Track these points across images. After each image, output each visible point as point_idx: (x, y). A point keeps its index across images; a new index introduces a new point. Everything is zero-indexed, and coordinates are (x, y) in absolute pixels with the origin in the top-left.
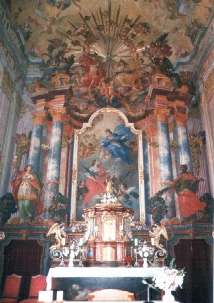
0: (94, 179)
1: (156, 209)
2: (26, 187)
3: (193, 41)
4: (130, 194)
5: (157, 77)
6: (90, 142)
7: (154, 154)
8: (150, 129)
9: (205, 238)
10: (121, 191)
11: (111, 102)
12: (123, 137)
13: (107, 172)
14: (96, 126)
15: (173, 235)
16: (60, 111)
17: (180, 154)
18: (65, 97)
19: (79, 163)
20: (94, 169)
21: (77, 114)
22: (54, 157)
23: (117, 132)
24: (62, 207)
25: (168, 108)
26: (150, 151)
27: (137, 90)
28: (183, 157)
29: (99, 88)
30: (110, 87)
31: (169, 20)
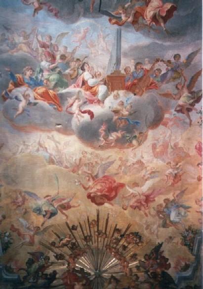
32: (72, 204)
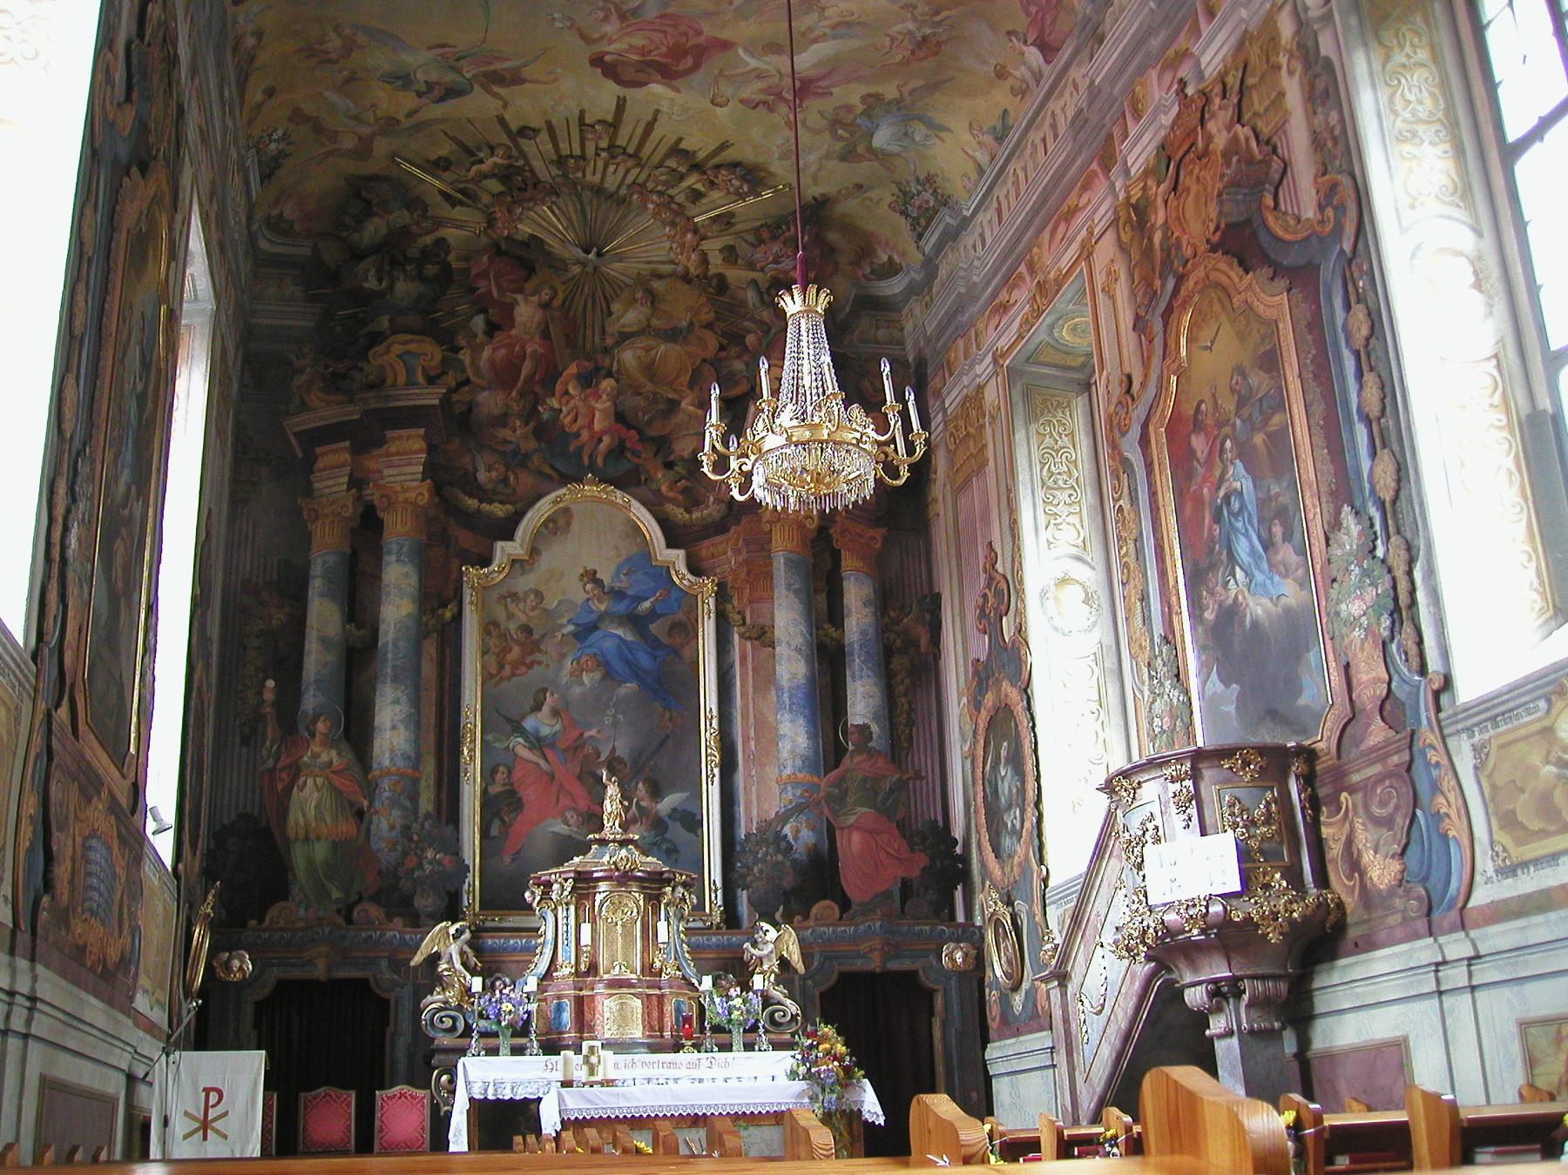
0: (542, 762)
1: (761, 871)
3: (920, 236)
4: (670, 816)
6: (523, 619)
8: (743, 575)
9: (918, 965)
11: (600, 461)
12: (647, 604)
14: (544, 554)
15: (817, 957)
16: (412, 495)
18: (426, 438)
20: (542, 723)
21: (472, 503)
23: (623, 583)
24: (440, 863)
28: (860, 689)
29: (556, 406)
30: (598, 405)
31: (832, 164)
32: (525, 73)
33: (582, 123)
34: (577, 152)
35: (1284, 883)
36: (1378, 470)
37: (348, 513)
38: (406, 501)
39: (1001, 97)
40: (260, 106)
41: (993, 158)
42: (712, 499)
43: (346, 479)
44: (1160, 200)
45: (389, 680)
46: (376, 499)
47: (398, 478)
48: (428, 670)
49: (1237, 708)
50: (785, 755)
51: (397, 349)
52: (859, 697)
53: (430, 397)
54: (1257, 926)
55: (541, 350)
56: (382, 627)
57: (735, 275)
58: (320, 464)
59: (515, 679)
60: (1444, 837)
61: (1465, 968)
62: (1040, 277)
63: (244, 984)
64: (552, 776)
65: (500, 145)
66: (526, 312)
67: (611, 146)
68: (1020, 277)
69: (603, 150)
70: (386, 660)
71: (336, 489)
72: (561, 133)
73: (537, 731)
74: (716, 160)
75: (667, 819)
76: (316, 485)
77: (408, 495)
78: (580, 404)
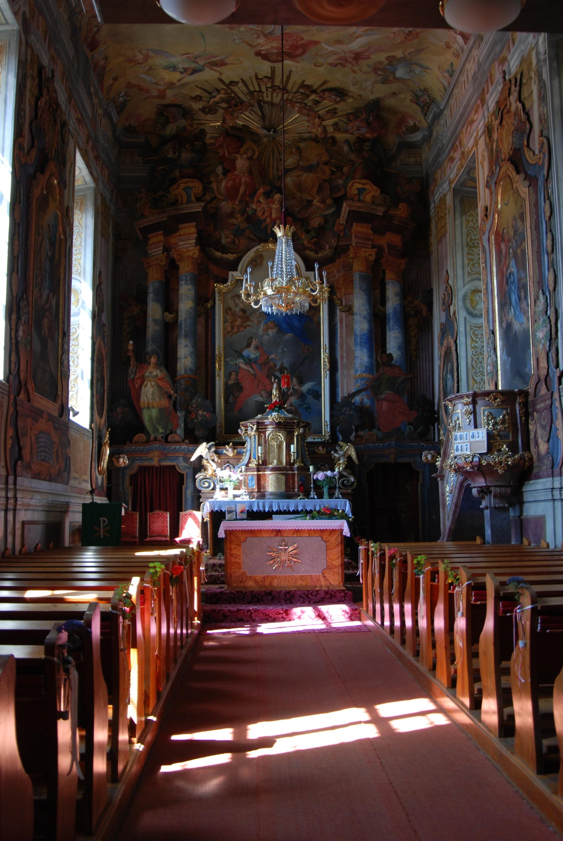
2: (152, 389)
3: (425, 115)
4: (307, 393)
5: (357, 186)
7: (346, 326)
10: (293, 388)
13: (271, 357)
16: (190, 253)
17: (387, 330)
18: (196, 226)
19: (228, 345)
20: (251, 353)
21: (219, 254)
22: (186, 337)
24: (204, 416)
25: (373, 247)
26: (341, 320)
27: (322, 205)
29: (254, 207)
30: (274, 206)
32: (227, 61)
33: (257, 78)
34: (257, 89)
35: (507, 449)
36: (550, 276)
37: (163, 263)
38: (189, 256)
39: (449, 57)
40: (111, 85)
41: (449, 84)
42: (327, 246)
43: (161, 248)
44: (496, 128)
45: (183, 337)
46: (175, 256)
47: (184, 246)
48: (201, 330)
49: (510, 367)
50: (357, 365)
51: (182, 186)
52: (392, 339)
53: (198, 208)
54: (494, 467)
55: (248, 180)
56: (180, 313)
57: (340, 136)
58: (151, 241)
59: (239, 333)
60: (557, 437)
61: (558, 492)
62: (463, 149)
63: (126, 468)
64: (255, 376)
65: (222, 89)
66: (241, 163)
67: (273, 86)
68: (457, 146)
69: (269, 88)
70: (182, 328)
71: (157, 253)
72: (249, 83)
73: (249, 356)
74: (324, 88)
75: (306, 394)
76: (149, 252)
77: (189, 253)
78: (265, 206)
